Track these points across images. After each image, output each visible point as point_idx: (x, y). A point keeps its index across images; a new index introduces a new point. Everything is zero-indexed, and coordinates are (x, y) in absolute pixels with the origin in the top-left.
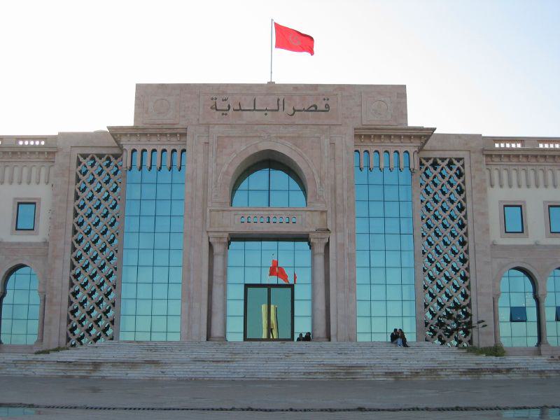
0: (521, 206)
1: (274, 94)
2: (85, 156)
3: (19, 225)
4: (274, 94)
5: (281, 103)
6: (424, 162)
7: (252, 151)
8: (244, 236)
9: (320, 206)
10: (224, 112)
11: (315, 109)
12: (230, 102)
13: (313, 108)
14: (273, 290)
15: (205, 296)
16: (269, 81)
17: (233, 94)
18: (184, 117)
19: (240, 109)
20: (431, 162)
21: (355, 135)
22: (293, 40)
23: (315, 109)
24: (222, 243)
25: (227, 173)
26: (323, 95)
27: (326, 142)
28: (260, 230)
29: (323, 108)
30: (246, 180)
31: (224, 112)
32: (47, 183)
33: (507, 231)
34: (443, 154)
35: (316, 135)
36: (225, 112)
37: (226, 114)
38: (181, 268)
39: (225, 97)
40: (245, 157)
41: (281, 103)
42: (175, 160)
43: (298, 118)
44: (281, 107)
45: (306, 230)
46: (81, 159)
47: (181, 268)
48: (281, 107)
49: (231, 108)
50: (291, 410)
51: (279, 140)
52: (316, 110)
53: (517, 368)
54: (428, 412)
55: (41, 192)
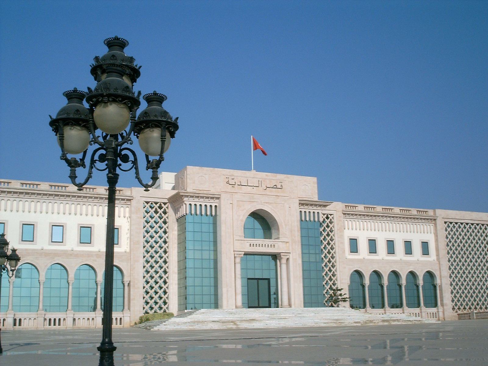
1: (257, 178)
3: (33, 227)
4: (257, 178)
5: (260, 182)
8: (218, 232)
11: (275, 187)
12: (236, 180)
13: (275, 187)
14: (260, 281)
17: (237, 176)
18: (213, 187)
21: (300, 204)
26: (279, 180)
27: (288, 206)
35: (283, 203)
36: (233, 186)
37: (234, 187)
38: (115, 243)
39: (233, 177)
41: (260, 182)
43: (268, 192)
44: (260, 185)
47: (115, 243)
48: (260, 185)
49: (236, 184)
51: (266, 204)
53: (465, 319)
54: (438, 235)
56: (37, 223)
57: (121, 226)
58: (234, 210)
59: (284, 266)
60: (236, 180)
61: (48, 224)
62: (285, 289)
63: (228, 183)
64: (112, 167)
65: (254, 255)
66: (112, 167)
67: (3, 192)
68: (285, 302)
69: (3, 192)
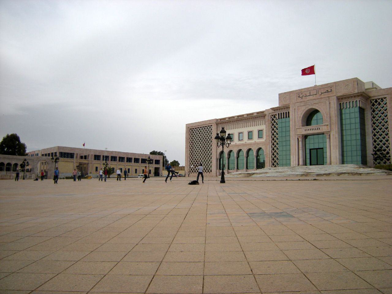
0: (259, 131)
2: (273, 115)
5: (317, 91)
6: (372, 101)
7: (307, 109)
9: (327, 124)
10: (302, 98)
11: (328, 91)
14: (318, 150)
15: (297, 153)
16: (315, 85)
19: (306, 96)
20: (375, 100)
22: (309, 71)
23: (328, 91)
24: (300, 138)
25: (300, 117)
28: (308, 133)
29: (330, 91)
30: (316, 115)
31: (302, 98)
32: (265, 124)
33: (312, 150)
34: (379, 97)
39: (302, 93)
40: (305, 111)
41: (317, 91)
42: (287, 115)
44: (318, 93)
45: (323, 131)
46: (272, 116)
48: (318, 93)
50: (325, 180)
52: (328, 92)
55: (263, 127)
56: (243, 132)
57: (253, 130)
58: (296, 112)
59: (328, 140)
60: (303, 94)
61: (247, 132)
62: (328, 154)
63: (299, 97)
64: (223, 145)
65: (313, 135)
66: (223, 145)
67: (391, 211)
68: (328, 161)
69: (391, 211)
